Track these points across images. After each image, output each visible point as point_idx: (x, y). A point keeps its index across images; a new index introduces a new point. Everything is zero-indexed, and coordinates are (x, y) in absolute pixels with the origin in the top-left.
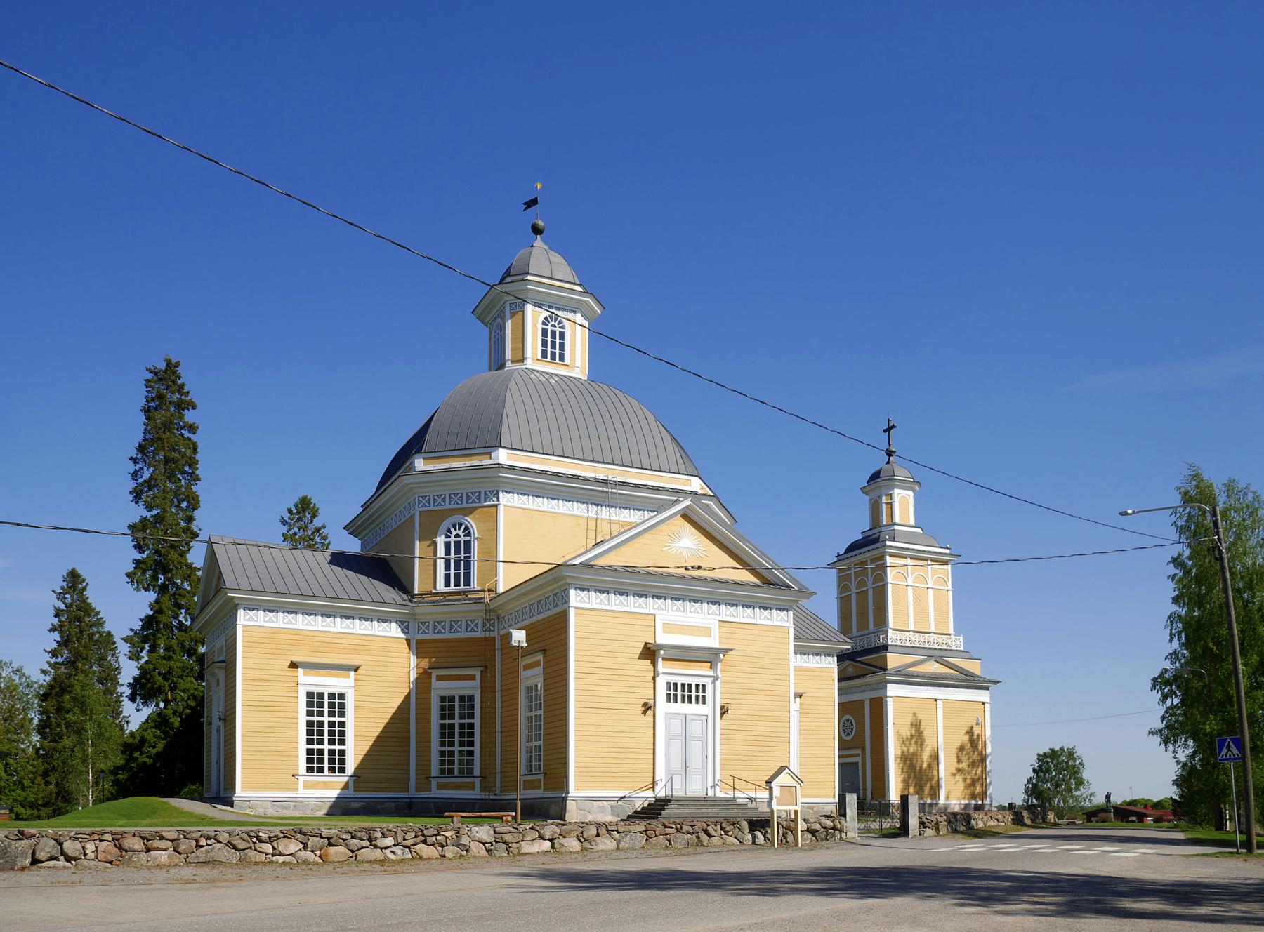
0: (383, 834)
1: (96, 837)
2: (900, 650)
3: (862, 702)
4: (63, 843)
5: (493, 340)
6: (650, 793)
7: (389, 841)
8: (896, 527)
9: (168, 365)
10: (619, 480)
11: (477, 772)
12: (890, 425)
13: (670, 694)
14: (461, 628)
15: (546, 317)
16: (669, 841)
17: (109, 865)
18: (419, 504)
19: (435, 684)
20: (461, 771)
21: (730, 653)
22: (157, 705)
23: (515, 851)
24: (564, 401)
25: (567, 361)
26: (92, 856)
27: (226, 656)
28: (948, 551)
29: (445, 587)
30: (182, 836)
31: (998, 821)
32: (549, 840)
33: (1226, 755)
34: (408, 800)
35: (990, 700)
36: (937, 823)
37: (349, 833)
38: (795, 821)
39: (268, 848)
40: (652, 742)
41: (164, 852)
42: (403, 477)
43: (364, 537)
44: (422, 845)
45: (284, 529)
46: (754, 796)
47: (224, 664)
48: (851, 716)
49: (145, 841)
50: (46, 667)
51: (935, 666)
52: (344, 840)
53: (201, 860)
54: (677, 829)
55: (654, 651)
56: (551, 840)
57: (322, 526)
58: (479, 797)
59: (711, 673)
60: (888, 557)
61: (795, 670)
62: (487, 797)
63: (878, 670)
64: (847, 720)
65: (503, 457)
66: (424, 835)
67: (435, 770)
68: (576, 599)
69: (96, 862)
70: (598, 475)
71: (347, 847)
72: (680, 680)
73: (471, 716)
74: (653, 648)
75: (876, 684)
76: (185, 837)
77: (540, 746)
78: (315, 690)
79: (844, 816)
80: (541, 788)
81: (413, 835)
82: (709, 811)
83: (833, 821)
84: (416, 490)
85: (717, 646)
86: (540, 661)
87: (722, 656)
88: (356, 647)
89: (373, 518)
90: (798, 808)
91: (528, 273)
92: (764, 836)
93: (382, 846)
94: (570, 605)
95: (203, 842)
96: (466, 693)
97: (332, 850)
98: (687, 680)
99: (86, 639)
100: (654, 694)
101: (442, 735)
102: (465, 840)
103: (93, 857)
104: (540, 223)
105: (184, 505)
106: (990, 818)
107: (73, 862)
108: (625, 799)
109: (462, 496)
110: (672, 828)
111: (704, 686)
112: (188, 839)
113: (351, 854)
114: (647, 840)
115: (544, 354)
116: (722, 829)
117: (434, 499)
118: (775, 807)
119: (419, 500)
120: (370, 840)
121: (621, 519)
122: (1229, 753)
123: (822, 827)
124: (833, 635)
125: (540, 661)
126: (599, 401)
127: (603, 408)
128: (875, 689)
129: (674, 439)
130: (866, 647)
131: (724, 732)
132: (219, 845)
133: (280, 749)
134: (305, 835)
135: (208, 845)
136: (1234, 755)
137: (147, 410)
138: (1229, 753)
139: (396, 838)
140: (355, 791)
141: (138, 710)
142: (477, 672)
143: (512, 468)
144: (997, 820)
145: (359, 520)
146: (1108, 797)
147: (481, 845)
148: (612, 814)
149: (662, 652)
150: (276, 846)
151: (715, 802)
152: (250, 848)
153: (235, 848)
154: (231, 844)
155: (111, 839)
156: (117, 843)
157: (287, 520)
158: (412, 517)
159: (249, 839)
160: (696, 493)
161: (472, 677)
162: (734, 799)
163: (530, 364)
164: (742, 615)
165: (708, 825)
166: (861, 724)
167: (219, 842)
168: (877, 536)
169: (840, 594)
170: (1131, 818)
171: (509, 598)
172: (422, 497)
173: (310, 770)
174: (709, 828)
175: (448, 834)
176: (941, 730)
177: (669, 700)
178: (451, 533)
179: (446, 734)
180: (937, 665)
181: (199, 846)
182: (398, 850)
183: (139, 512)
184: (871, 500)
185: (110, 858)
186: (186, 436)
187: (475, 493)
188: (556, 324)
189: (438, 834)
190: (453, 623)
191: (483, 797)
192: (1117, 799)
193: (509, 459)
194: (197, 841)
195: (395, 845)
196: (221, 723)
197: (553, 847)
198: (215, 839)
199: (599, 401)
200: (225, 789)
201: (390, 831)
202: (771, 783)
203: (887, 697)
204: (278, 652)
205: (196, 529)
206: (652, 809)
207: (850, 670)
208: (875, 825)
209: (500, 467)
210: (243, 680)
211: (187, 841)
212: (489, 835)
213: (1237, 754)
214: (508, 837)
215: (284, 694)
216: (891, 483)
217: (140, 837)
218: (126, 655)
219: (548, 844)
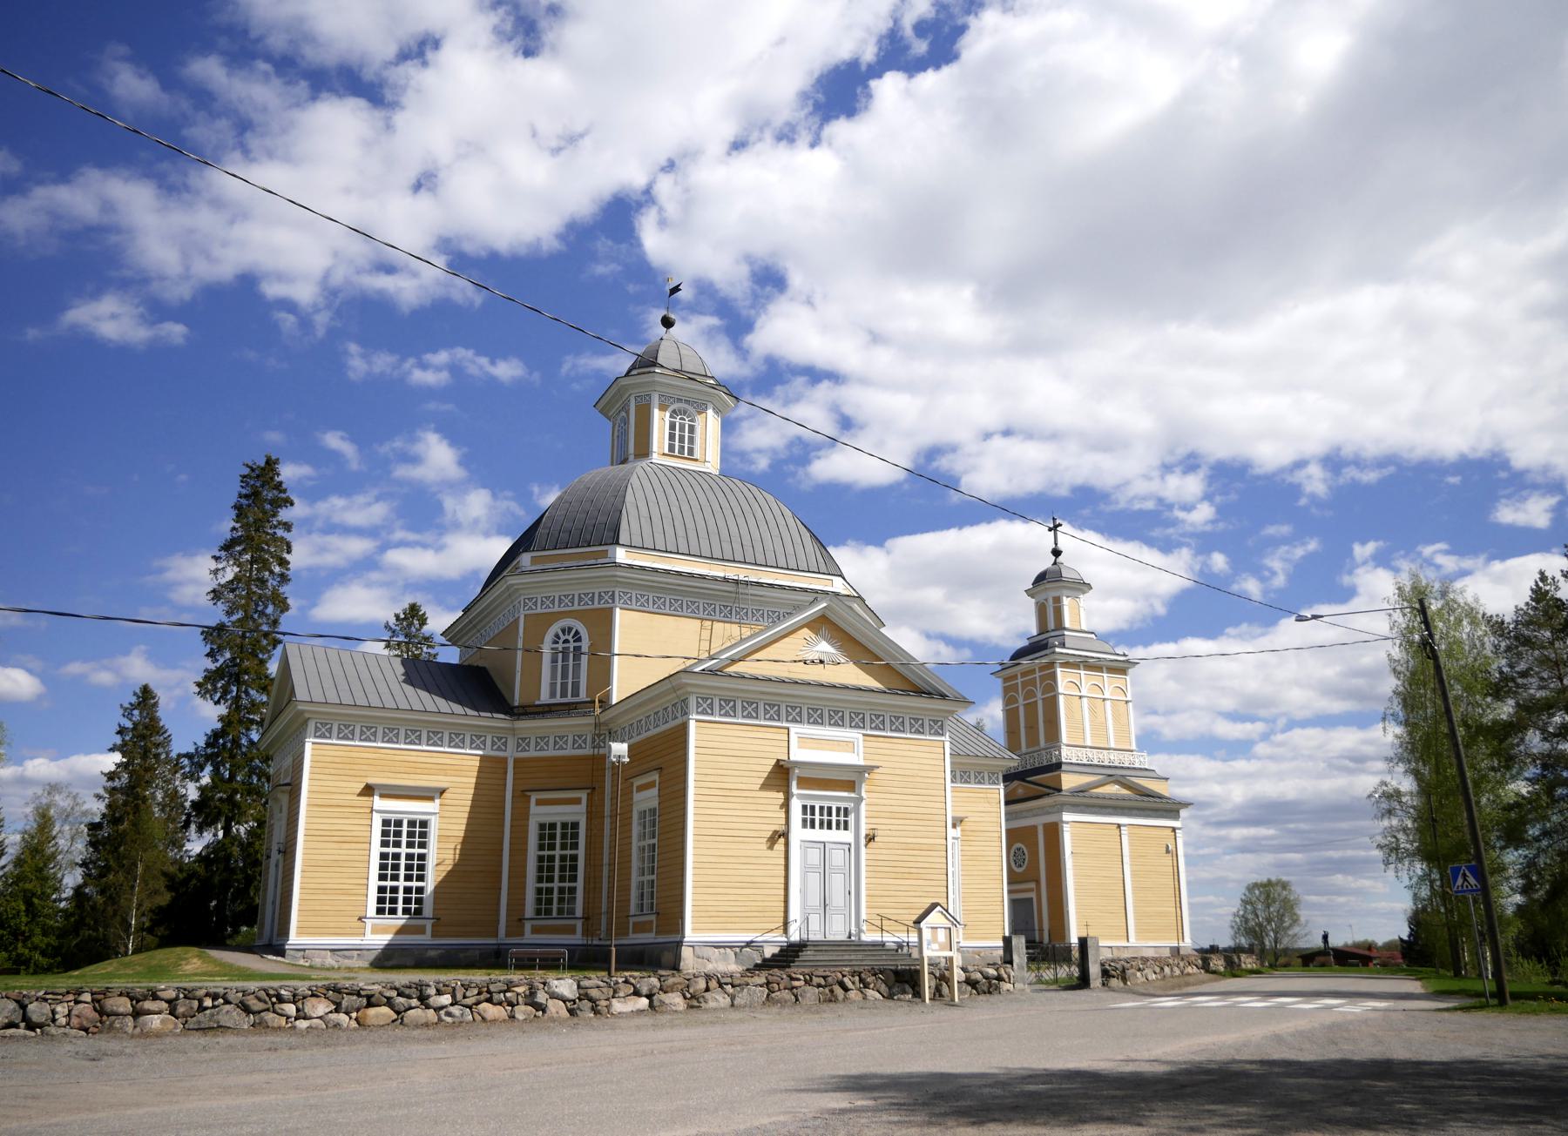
0: (437, 990)
1: (71, 997)
3: (1034, 828)
4: (27, 1006)
5: (616, 434)
7: (446, 999)
8: (1066, 633)
11: (579, 912)
16: (796, 996)
17: (83, 1033)
19: (534, 809)
20: (560, 911)
21: (876, 771)
22: (215, 835)
25: (697, 455)
26: (63, 1021)
33: (1462, 886)
34: (495, 947)
38: (950, 968)
39: (291, 1009)
41: (156, 1016)
44: (485, 1005)
46: (906, 940)
47: (289, 788)
49: (134, 1002)
50: (101, 792)
53: (202, 1026)
54: (805, 981)
55: (788, 769)
56: (650, 996)
58: (580, 942)
62: (590, 942)
64: (1019, 849)
65: (622, 555)
67: (529, 910)
69: (67, 1030)
74: (786, 765)
76: (185, 997)
79: (1011, 962)
81: (476, 991)
82: (853, 957)
83: (997, 970)
84: (522, 592)
85: (862, 763)
87: (867, 775)
88: (445, 767)
95: (208, 1002)
96: (569, 819)
97: (372, 1011)
98: (826, 804)
99: (1449, 757)
101: (540, 869)
102: (541, 997)
103: (64, 1023)
107: (38, 1030)
110: (799, 980)
112: (189, 999)
113: (395, 1016)
114: (768, 995)
115: (671, 448)
116: (861, 980)
118: (927, 953)
122: (1466, 883)
127: (734, 503)
128: (1049, 813)
129: (813, 535)
130: (1037, 765)
131: (697, 871)
134: (340, 993)
135: (214, 1007)
137: (238, 507)
138: (1466, 883)
139: (454, 996)
140: (432, 936)
142: (583, 795)
143: (631, 567)
146: (1325, 937)
147: (561, 1003)
148: (736, 963)
156: (97, 1005)
158: (517, 621)
159: (267, 999)
160: (837, 594)
161: (577, 801)
162: (883, 944)
163: (656, 458)
165: (844, 976)
166: (1035, 854)
168: (1045, 642)
171: (622, 709)
173: (380, 911)
174: (846, 980)
175: (520, 990)
176: (1126, 859)
177: (804, 826)
178: (559, 638)
179: (545, 866)
181: (202, 1009)
182: (456, 1010)
185: (85, 1023)
189: (508, 990)
192: (1337, 941)
194: (201, 1001)
195: (452, 1005)
196: (280, 857)
197: (651, 1005)
200: (278, 935)
201: (447, 986)
203: (1063, 822)
206: (783, 956)
207: (1020, 791)
208: (1048, 974)
209: (619, 566)
210: (309, 805)
211: (188, 1001)
212: (572, 992)
214: (594, 993)
215: (356, 822)
217: (128, 996)
219: (644, 1002)
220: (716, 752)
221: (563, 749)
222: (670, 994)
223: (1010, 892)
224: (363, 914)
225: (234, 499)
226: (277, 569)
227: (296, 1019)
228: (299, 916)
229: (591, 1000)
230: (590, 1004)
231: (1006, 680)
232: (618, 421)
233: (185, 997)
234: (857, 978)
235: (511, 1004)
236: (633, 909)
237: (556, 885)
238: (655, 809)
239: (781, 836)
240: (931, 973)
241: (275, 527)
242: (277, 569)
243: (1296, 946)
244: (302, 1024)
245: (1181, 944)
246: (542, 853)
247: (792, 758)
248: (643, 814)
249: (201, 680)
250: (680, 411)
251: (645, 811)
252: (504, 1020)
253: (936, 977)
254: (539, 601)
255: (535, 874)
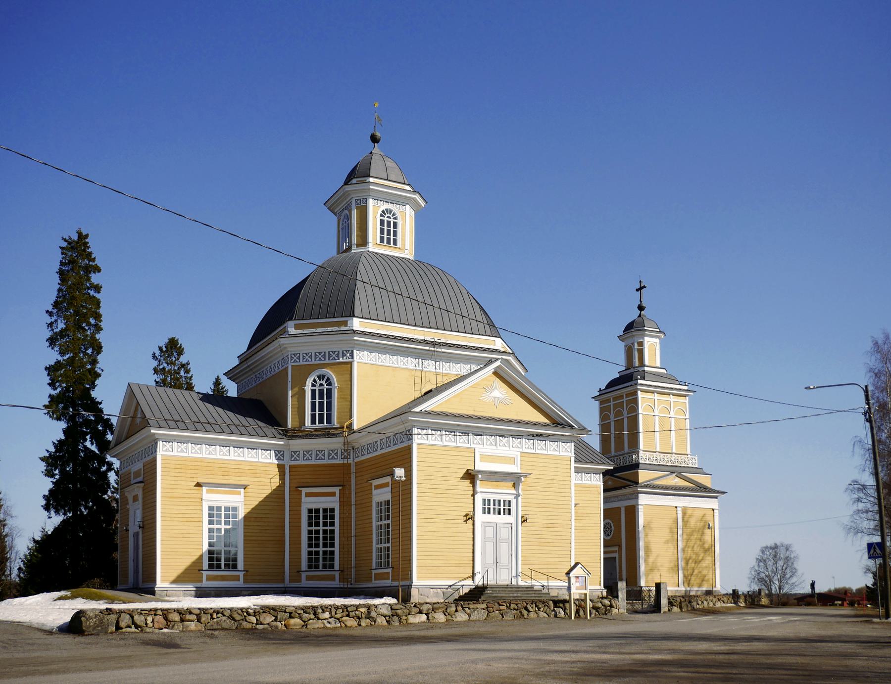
2: (648, 467)
3: (619, 509)
5: (341, 227)
6: (469, 582)
7: (327, 615)
8: (646, 369)
9: (79, 237)
10: (442, 341)
12: (642, 285)
13: (485, 508)
14: (324, 456)
15: (383, 210)
18: (291, 360)
19: (304, 499)
20: (324, 566)
21: (529, 476)
23: (405, 622)
24: (400, 279)
26: (151, 625)
27: (144, 478)
28: (686, 388)
29: (312, 424)
30: (202, 612)
31: (724, 603)
32: (426, 614)
33: (873, 554)
34: (284, 589)
35: (719, 507)
36: (681, 603)
37: (302, 609)
38: (584, 600)
39: (253, 619)
40: (472, 544)
41: (192, 622)
42: (280, 339)
43: (240, 382)
45: (155, 363)
46: (546, 584)
48: (611, 520)
51: (676, 480)
52: (299, 614)
54: (507, 606)
55: (474, 476)
57: (187, 363)
58: (338, 586)
59: (514, 492)
60: (639, 392)
61: (575, 487)
62: (346, 586)
63: (632, 484)
65: (357, 324)
66: (347, 611)
67: (304, 565)
68: (419, 439)
70: (426, 338)
71: (301, 618)
72: (492, 497)
73: (332, 524)
75: (630, 494)
76: (204, 613)
77: (388, 548)
78: (215, 504)
80: (389, 579)
83: (610, 601)
85: (519, 471)
86: (388, 483)
89: (251, 368)
90: (587, 592)
91: (369, 176)
92: (564, 612)
93: (322, 618)
94: (414, 442)
96: (328, 506)
98: (497, 497)
100: (474, 507)
101: (310, 539)
104: (378, 134)
105: (89, 351)
106: (717, 600)
107: (140, 629)
108: (453, 587)
109: (325, 355)
111: (509, 502)
112: (206, 613)
114: (488, 614)
117: (303, 356)
119: (291, 357)
120: (315, 614)
121: (444, 371)
123: (603, 605)
124: (600, 458)
125: (388, 483)
126: (425, 279)
127: (428, 284)
130: (622, 465)
132: (224, 618)
133: (189, 550)
135: (217, 618)
136: (878, 554)
137: (61, 273)
139: (331, 613)
141: (49, 518)
142: (337, 490)
143: (364, 333)
144: (723, 601)
145: (238, 369)
146: (813, 585)
147: (383, 618)
149: (480, 476)
150: (258, 618)
151: (518, 588)
152: (243, 620)
153: (234, 619)
154: (232, 617)
155: (161, 614)
157: (157, 356)
162: (532, 586)
163: (372, 247)
164: (539, 446)
166: (619, 528)
167: (224, 615)
169: (602, 422)
170: (836, 602)
172: (294, 354)
177: (484, 513)
178: (316, 383)
180: (677, 480)
183: (53, 356)
184: (626, 346)
186: (91, 294)
187: (335, 352)
188: (391, 216)
190: (318, 452)
191: (342, 586)
192: (820, 588)
193: (361, 326)
194: (211, 615)
195: (330, 618)
196: (140, 531)
197: (428, 619)
198: (222, 614)
199: (425, 279)
200: (143, 582)
202: (569, 574)
204: (188, 475)
205: (99, 371)
209: (355, 332)
210: (162, 497)
212: (388, 611)
213: (880, 554)
214: (399, 612)
216: (643, 333)
217: (178, 612)
218: (43, 472)
220: (429, 464)
221: (322, 459)
222: (437, 613)
223: (605, 553)
224: (200, 568)
225: (57, 266)
226: (92, 321)
227: (257, 624)
228: (161, 569)
229: (398, 616)
230: (397, 618)
231: (601, 403)
232: (342, 217)
233: (204, 613)
234: (534, 605)
235: (359, 618)
236: (374, 566)
237: (321, 549)
238: (389, 501)
239: (470, 518)
240: (574, 603)
241: (88, 288)
242: (92, 321)
243: (793, 593)
244: (260, 627)
245: (714, 589)
246: (310, 528)
247: (477, 468)
248: (380, 504)
249: (47, 403)
250: (391, 212)
251: (381, 503)
252: (356, 626)
253: (576, 605)
254: (301, 357)
255: (307, 542)
